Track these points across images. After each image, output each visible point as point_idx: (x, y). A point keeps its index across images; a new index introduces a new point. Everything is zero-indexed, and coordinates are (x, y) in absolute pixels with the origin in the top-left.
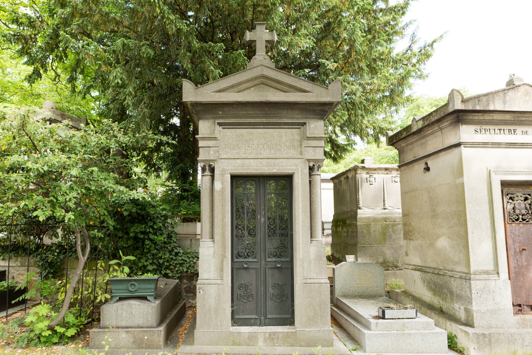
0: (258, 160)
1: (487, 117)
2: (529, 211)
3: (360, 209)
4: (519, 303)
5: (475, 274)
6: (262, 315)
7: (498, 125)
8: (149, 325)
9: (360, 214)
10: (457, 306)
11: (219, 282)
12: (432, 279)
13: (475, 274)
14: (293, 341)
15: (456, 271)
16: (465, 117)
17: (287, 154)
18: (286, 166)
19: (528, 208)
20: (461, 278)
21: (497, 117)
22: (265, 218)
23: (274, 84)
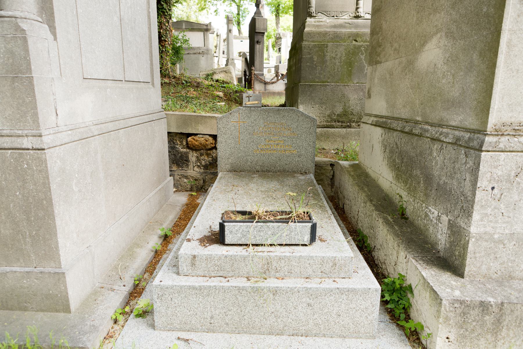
3: (311, 16)
5: (499, 133)
9: (309, 26)
10: (434, 212)
12: (399, 143)
13: (499, 133)
15: (448, 126)
20: (457, 143)
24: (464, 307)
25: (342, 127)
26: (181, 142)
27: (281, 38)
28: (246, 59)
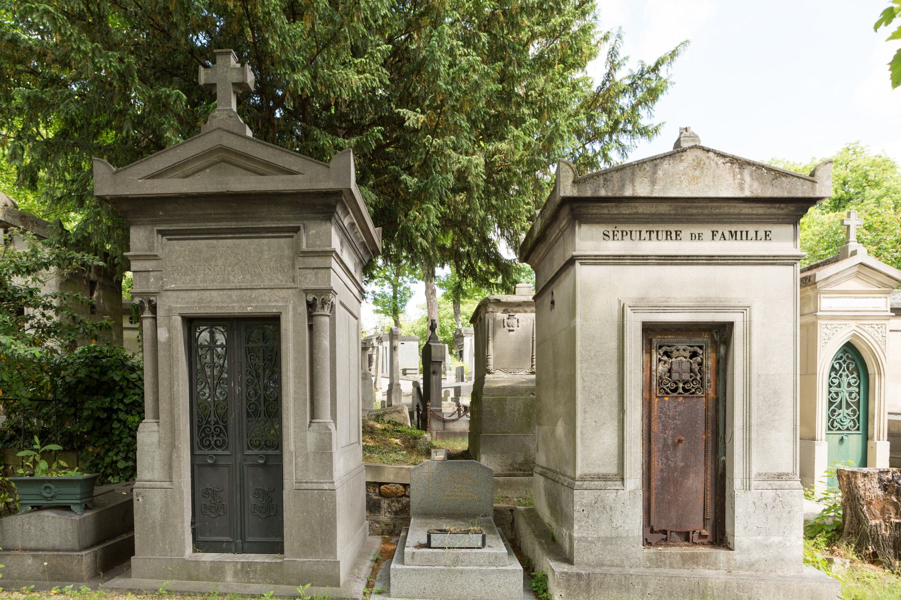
0: (225, 292)
1: (625, 210)
2: (696, 375)
3: (489, 373)
4: (663, 528)
6: (239, 537)
7: (648, 223)
8: (69, 547)
9: (488, 381)
11: (166, 484)
13: (583, 479)
14: (271, 575)
16: (584, 210)
17: (270, 280)
18: (270, 301)
19: (697, 370)
21: (642, 209)
22: (241, 386)
23: (242, 162)
24: (568, 576)
25: (524, 475)
26: (374, 490)
27: (463, 337)
28: (418, 389)
